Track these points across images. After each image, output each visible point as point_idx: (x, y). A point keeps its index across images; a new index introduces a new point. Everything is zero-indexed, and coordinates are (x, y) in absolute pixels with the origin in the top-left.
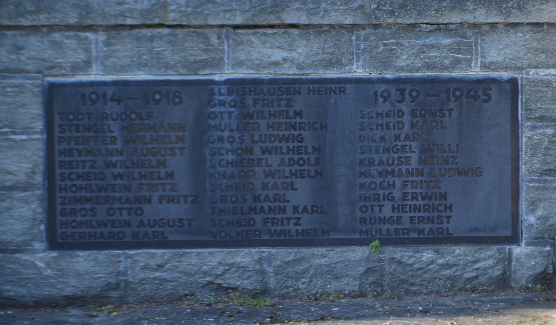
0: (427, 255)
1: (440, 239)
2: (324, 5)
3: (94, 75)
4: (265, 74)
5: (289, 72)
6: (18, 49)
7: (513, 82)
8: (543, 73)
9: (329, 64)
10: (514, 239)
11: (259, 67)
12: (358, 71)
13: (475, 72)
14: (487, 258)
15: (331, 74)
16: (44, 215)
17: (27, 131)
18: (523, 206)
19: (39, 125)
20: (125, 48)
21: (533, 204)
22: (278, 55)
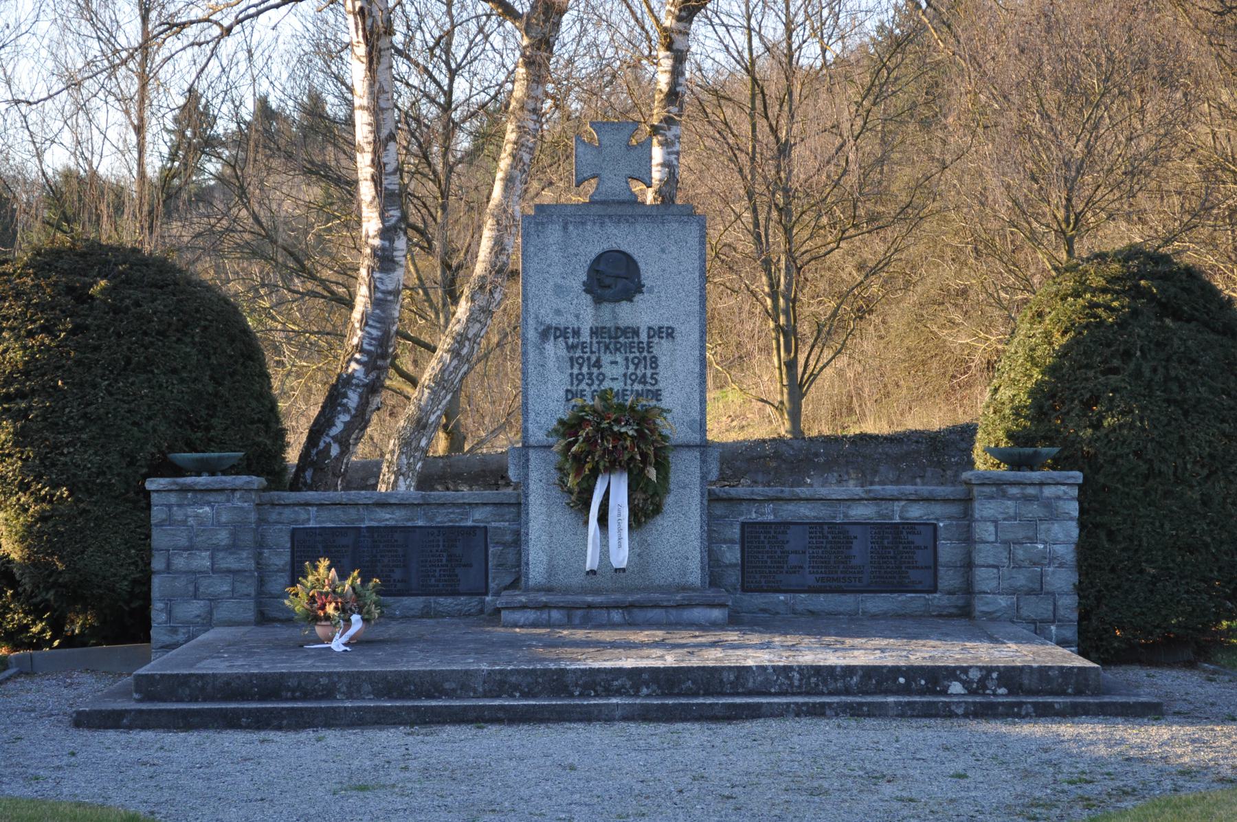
0: (450, 600)
1: (455, 593)
2: (1230, 43)
3: (312, 524)
4: (382, 524)
5: (393, 523)
6: (280, 514)
7: (486, 528)
8: (497, 524)
9: (409, 520)
10: (486, 594)
11: (380, 521)
12: (420, 523)
13: (470, 523)
14: (475, 601)
15: (409, 524)
16: (639, 228)
17: (283, 547)
18: (490, 579)
19: (289, 545)
20: (325, 514)
21: (494, 579)
22: (388, 516)
